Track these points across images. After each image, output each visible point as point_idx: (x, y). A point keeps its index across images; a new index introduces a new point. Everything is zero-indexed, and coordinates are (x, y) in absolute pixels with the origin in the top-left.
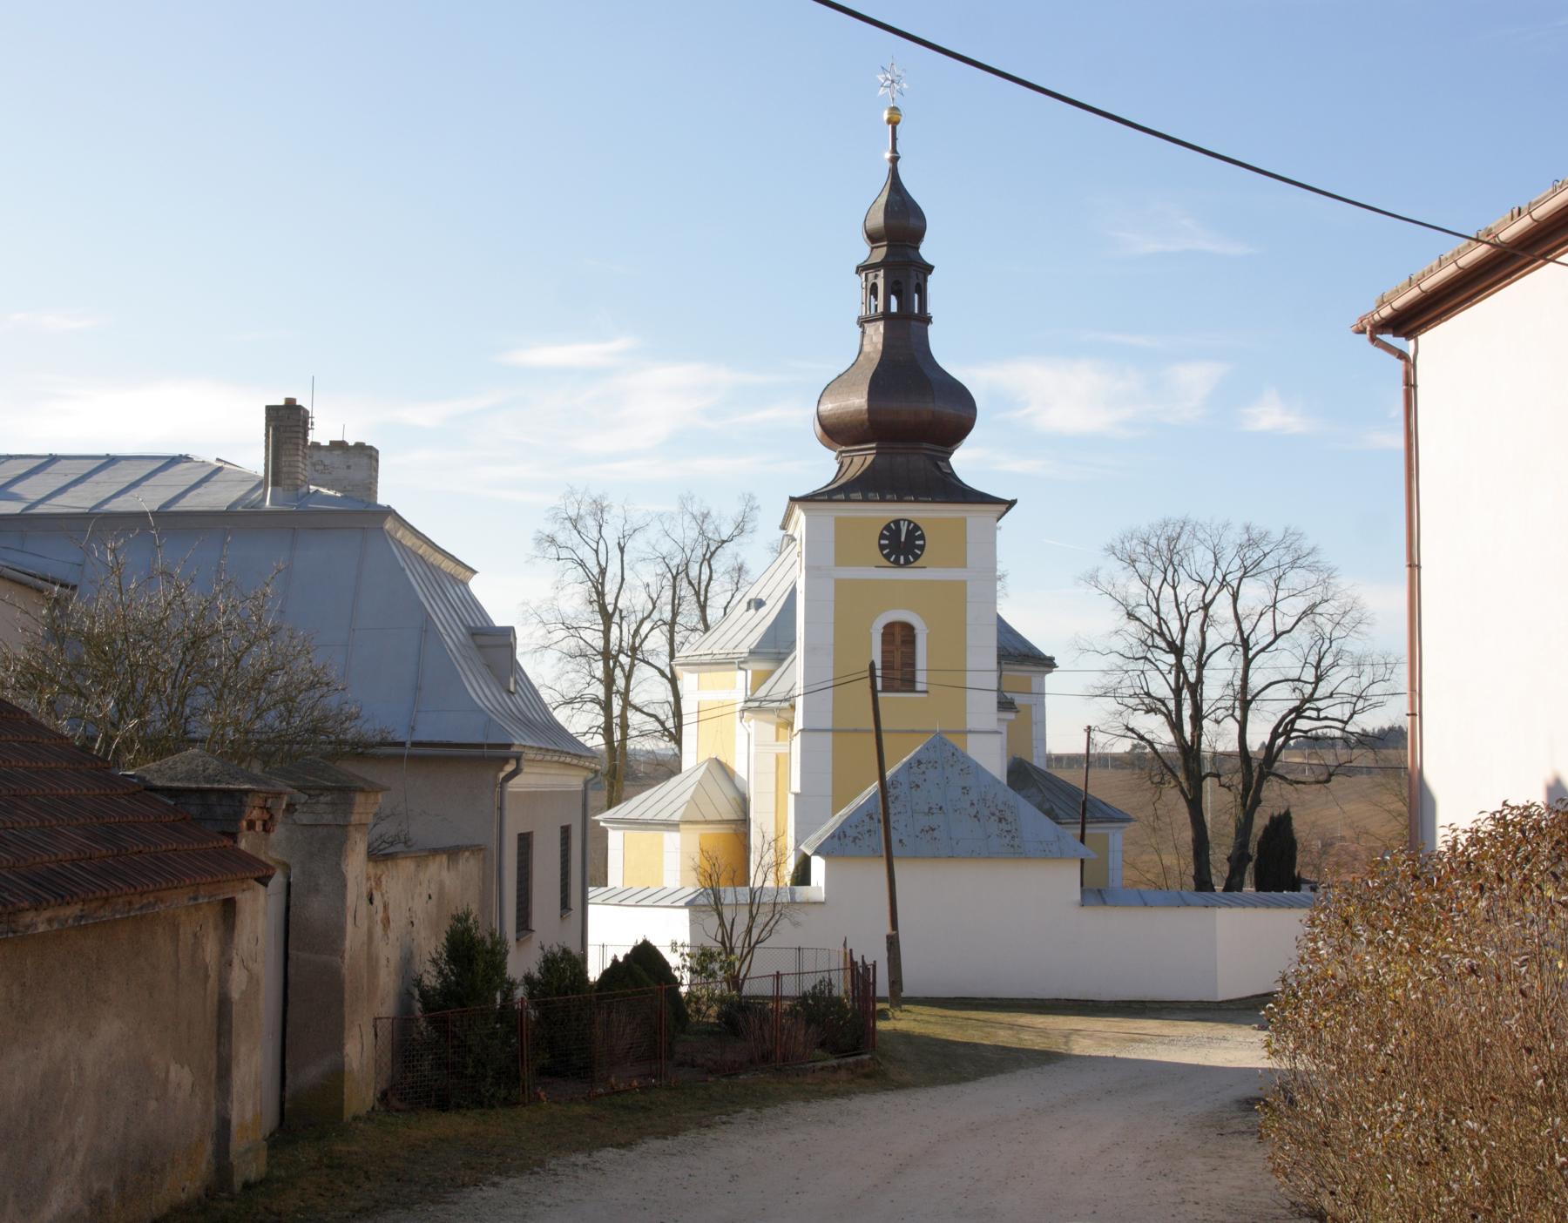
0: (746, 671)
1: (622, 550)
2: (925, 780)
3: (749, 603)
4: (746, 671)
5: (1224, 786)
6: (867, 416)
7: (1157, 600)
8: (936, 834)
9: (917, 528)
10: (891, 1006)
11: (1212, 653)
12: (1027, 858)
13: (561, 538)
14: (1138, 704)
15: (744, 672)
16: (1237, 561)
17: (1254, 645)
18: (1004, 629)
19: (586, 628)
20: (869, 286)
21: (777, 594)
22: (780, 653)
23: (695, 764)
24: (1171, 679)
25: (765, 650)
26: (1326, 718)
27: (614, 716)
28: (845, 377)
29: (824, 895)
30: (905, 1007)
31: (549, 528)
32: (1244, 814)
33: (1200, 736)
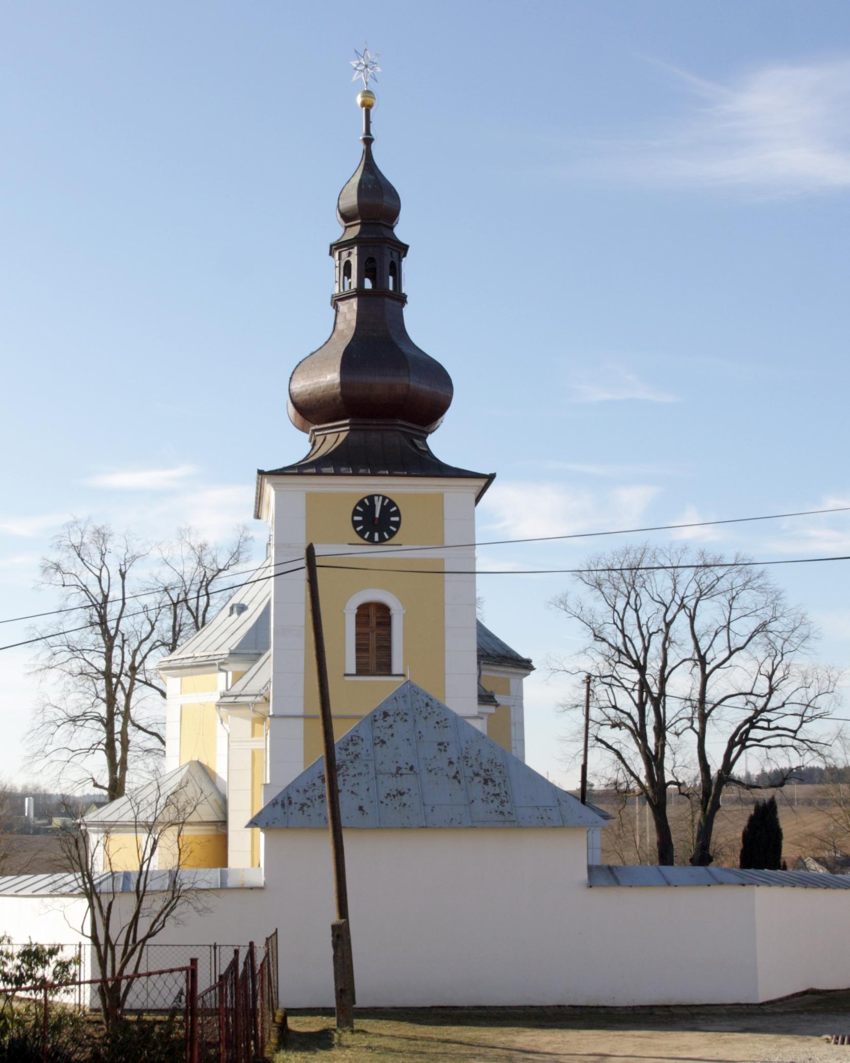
0: (226, 672)
1: (123, 576)
2: (392, 735)
3: (232, 609)
4: (226, 672)
5: (683, 794)
6: (339, 390)
7: (622, 620)
8: (405, 799)
9: (392, 504)
10: (338, 1025)
11: (673, 669)
12: (520, 827)
13: (65, 566)
14: (605, 720)
15: (224, 674)
16: (694, 586)
17: (712, 660)
18: (483, 634)
19: (91, 650)
20: (343, 264)
21: (259, 599)
23: (178, 767)
24: (636, 695)
25: (245, 651)
26: (777, 728)
27: (115, 732)
28: (317, 354)
29: (263, 879)
30: (359, 1024)
31: (55, 557)
32: (704, 818)
33: (663, 746)
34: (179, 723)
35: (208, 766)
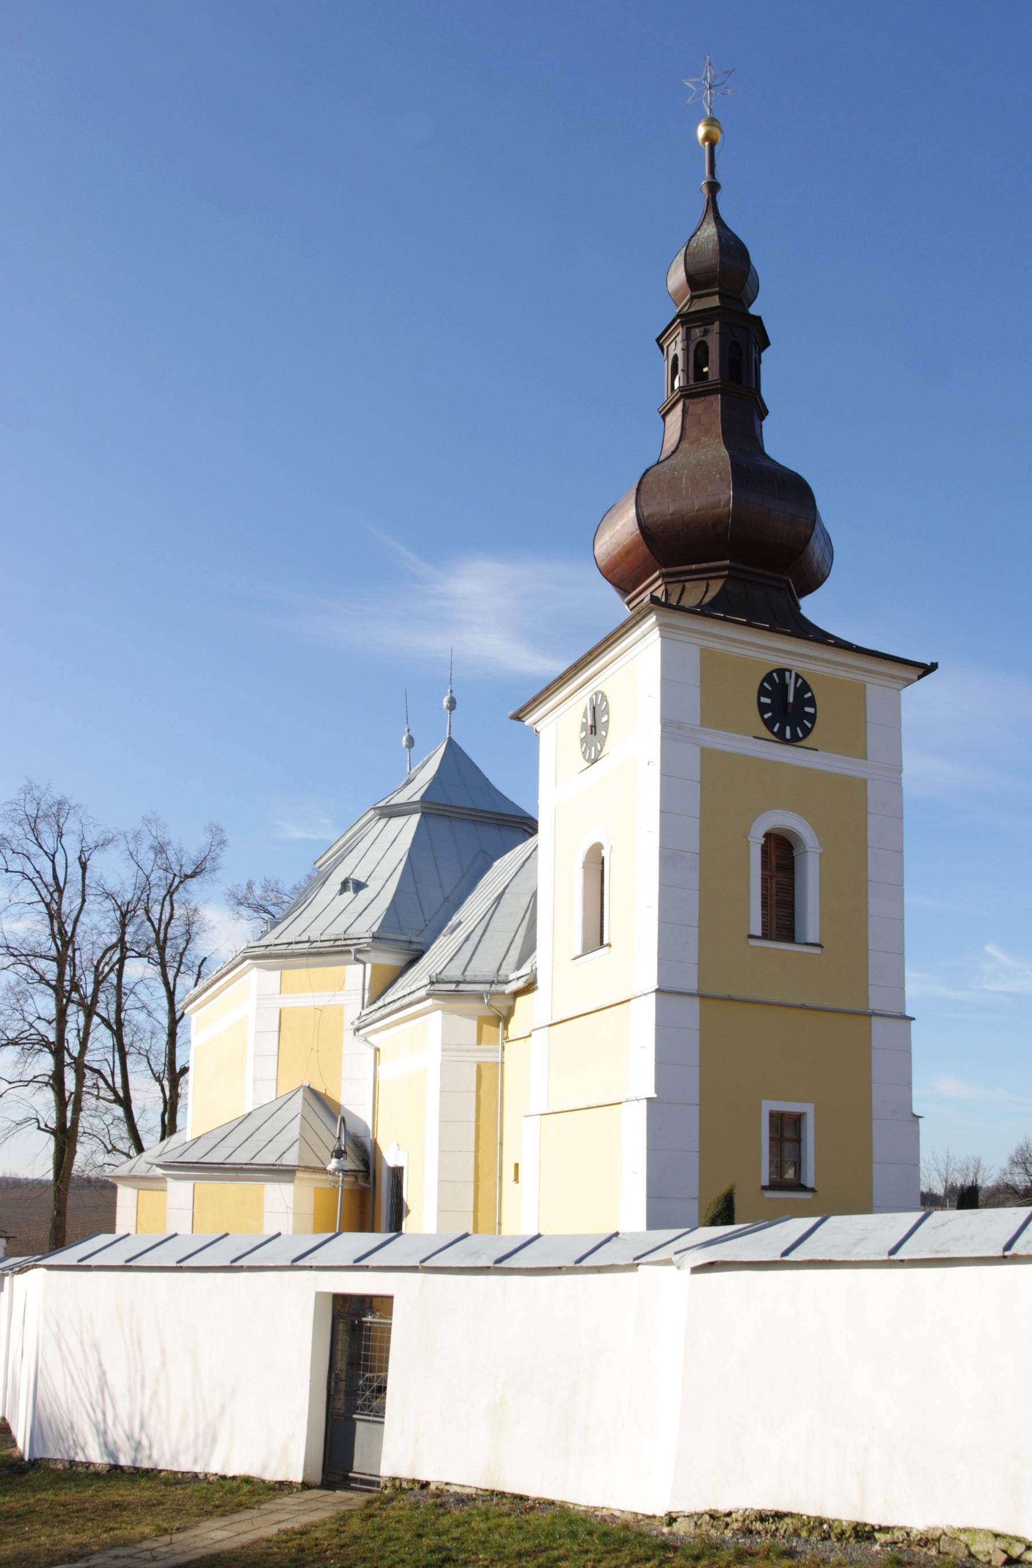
0: (364, 963)
1: (84, 867)
15: (361, 966)
21: (383, 871)
22: (411, 942)
34: (277, 1033)
35: (325, 1095)
